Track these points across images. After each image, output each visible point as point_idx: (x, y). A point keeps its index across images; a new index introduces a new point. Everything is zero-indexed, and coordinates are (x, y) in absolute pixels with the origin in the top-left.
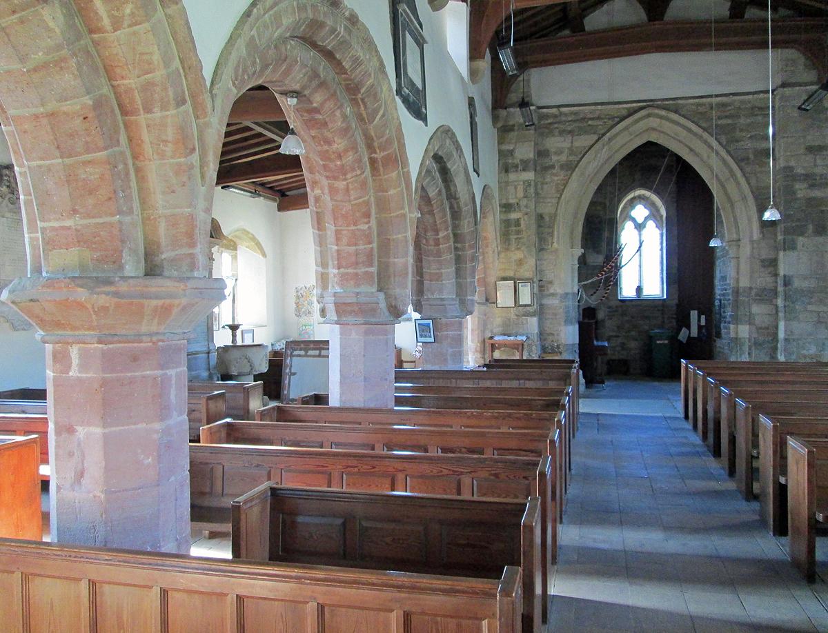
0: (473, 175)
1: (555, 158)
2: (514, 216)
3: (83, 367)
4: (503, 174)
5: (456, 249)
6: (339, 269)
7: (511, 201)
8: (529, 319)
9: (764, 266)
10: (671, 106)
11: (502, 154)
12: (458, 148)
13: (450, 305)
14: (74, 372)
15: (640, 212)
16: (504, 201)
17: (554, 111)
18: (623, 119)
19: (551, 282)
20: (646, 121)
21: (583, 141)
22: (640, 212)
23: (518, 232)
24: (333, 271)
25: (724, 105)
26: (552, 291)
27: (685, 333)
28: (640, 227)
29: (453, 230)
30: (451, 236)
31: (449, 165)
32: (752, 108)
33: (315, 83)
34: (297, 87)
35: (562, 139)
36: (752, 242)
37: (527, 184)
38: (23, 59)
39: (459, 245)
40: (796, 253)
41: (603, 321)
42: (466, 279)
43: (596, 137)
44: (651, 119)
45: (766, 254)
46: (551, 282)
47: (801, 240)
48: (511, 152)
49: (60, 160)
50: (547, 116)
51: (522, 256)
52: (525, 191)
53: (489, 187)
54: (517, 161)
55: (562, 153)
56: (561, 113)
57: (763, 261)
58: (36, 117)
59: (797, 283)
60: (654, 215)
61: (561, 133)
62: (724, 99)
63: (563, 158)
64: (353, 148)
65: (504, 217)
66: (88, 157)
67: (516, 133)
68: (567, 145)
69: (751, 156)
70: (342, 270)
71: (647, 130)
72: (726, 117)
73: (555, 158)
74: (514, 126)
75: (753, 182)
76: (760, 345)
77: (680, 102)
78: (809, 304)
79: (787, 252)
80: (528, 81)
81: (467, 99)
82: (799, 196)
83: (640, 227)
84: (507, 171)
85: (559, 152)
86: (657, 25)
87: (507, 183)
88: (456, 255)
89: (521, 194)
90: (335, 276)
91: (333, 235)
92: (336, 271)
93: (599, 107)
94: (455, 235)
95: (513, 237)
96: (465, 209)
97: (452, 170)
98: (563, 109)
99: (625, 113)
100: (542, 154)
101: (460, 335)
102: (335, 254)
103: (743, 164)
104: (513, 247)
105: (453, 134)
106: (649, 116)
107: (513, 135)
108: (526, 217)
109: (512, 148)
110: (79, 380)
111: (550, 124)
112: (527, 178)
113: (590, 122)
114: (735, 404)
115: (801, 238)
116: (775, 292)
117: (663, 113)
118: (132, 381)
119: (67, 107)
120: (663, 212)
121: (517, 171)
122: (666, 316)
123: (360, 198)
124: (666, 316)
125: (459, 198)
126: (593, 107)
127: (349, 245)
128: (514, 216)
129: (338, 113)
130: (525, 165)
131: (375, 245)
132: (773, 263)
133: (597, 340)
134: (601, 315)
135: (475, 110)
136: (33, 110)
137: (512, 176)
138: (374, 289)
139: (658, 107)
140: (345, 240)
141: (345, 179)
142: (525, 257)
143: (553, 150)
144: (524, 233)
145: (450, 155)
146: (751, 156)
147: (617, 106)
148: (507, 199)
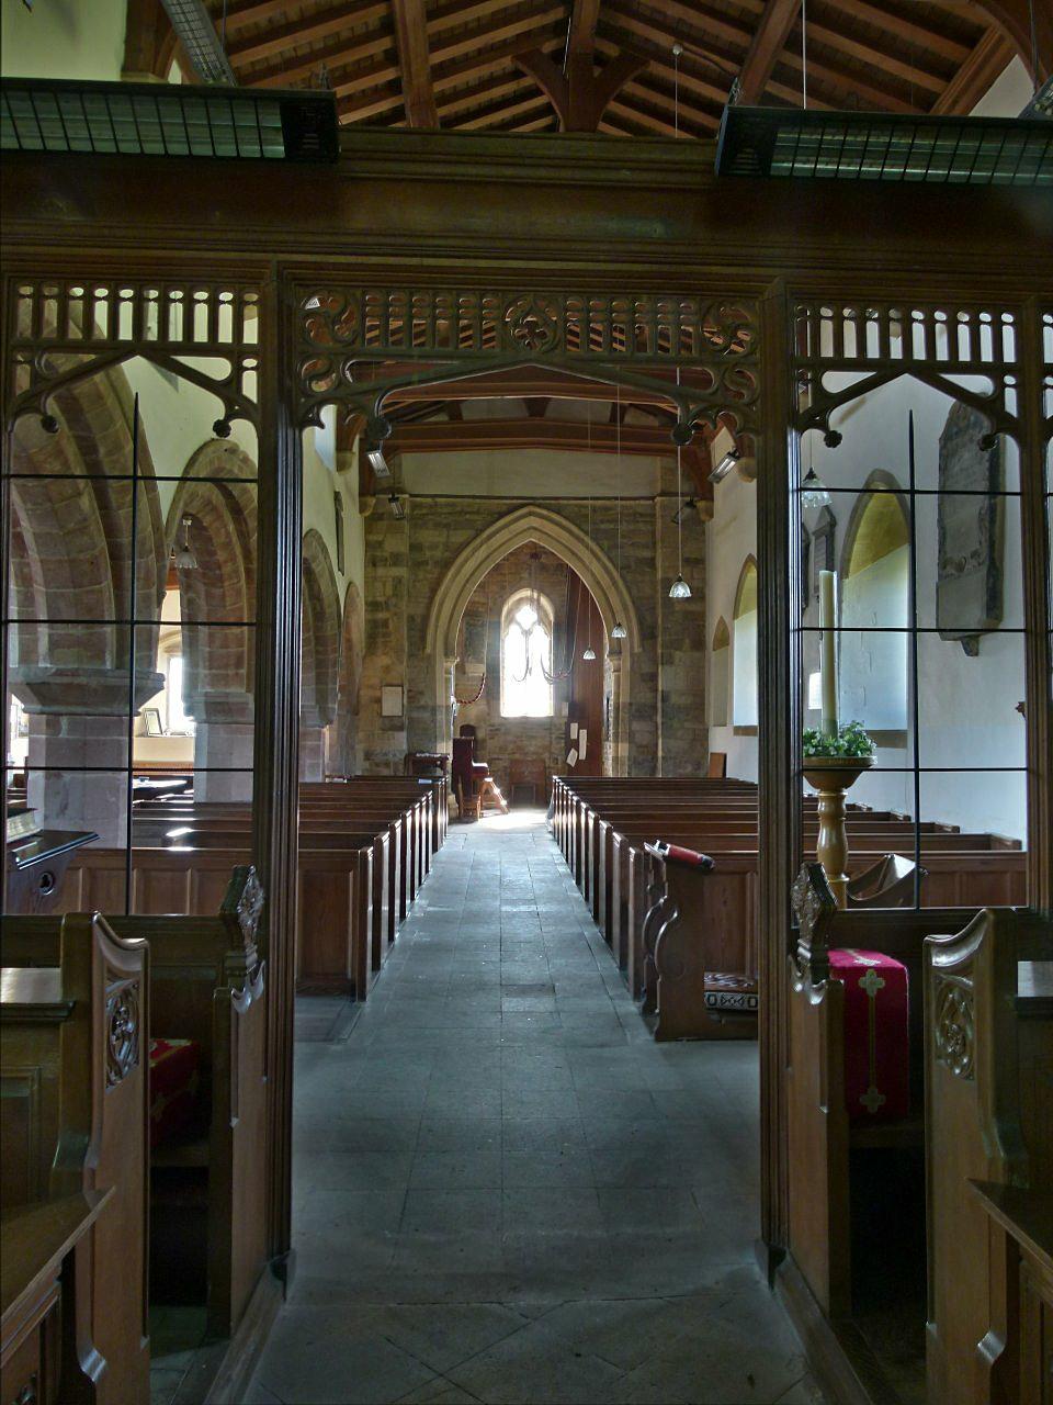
0: (337, 574)
1: (428, 554)
2: (381, 616)
3: (70, 731)
4: (370, 569)
5: (317, 652)
6: (210, 669)
7: (379, 599)
8: (396, 734)
9: (644, 681)
10: (553, 505)
11: (368, 545)
12: (324, 549)
13: (955, 102)
14: (63, 735)
15: (526, 615)
16: (370, 599)
17: (429, 500)
18: (501, 515)
19: (422, 693)
20: (526, 519)
21: (459, 537)
22: (526, 615)
23: (386, 635)
24: (203, 672)
25: (607, 509)
26: (422, 703)
27: (574, 754)
28: (527, 633)
29: (314, 632)
30: (312, 638)
31: (313, 565)
32: (635, 515)
33: (208, 508)
34: (194, 512)
35: (437, 533)
36: (632, 655)
37: (398, 581)
38: (61, 527)
39: (321, 649)
40: (673, 668)
41: (484, 741)
42: (327, 684)
43: (471, 533)
44: (532, 517)
45: (646, 669)
46: (422, 693)
47: (678, 655)
48: (380, 544)
49: (72, 590)
50: (420, 506)
51: (390, 662)
52: (395, 588)
53: (355, 586)
54: (386, 554)
55: (437, 547)
56: (436, 504)
57: (642, 675)
58: (60, 561)
59: (674, 699)
60: (542, 620)
61: (437, 525)
62: (608, 503)
63: (438, 554)
64: (231, 560)
65: (369, 617)
66: (89, 588)
67: (385, 522)
68: (442, 539)
69: (633, 564)
70: (214, 671)
71: (529, 529)
72: (608, 521)
73: (428, 554)
74: (383, 514)
75: (634, 591)
76: (639, 764)
77: (561, 502)
78: (686, 720)
79: (666, 667)
80: (400, 466)
81: (333, 495)
82: (677, 609)
83: (527, 633)
84: (374, 565)
85: (434, 547)
86: (537, 421)
87: (375, 579)
88: (317, 659)
89: (389, 591)
90: (206, 676)
91: (207, 638)
92: (207, 672)
93: (478, 501)
94: (317, 638)
95: (380, 640)
96: (328, 611)
97: (316, 571)
98: (438, 500)
99: (504, 509)
100: (415, 547)
101: (319, 746)
102: (207, 655)
103: (625, 572)
104: (380, 652)
105: (320, 537)
106: (530, 514)
107: (383, 524)
108: (395, 618)
109: (380, 539)
110: (68, 740)
111: (424, 515)
112: (397, 574)
113: (468, 516)
114: (599, 824)
115: (677, 652)
116: (654, 707)
117: (545, 512)
118: (105, 743)
119: (82, 556)
120: (552, 618)
121: (385, 565)
122: (553, 736)
123: (235, 604)
124: (553, 736)
125: (322, 599)
126: (471, 500)
127: (221, 648)
128: (381, 616)
129: (223, 530)
130: (396, 560)
131: (246, 648)
132: (653, 677)
133: (475, 762)
134: (481, 734)
135: (341, 505)
136: (58, 557)
137: (381, 571)
138: (243, 691)
139: (539, 506)
140: (218, 643)
141: (222, 587)
142: (393, 663)
143: (427, 544)
144: (393, 637)
145: (315, 558)
146: (633, 564)
147: (496, 501)
148: (374, 597)
